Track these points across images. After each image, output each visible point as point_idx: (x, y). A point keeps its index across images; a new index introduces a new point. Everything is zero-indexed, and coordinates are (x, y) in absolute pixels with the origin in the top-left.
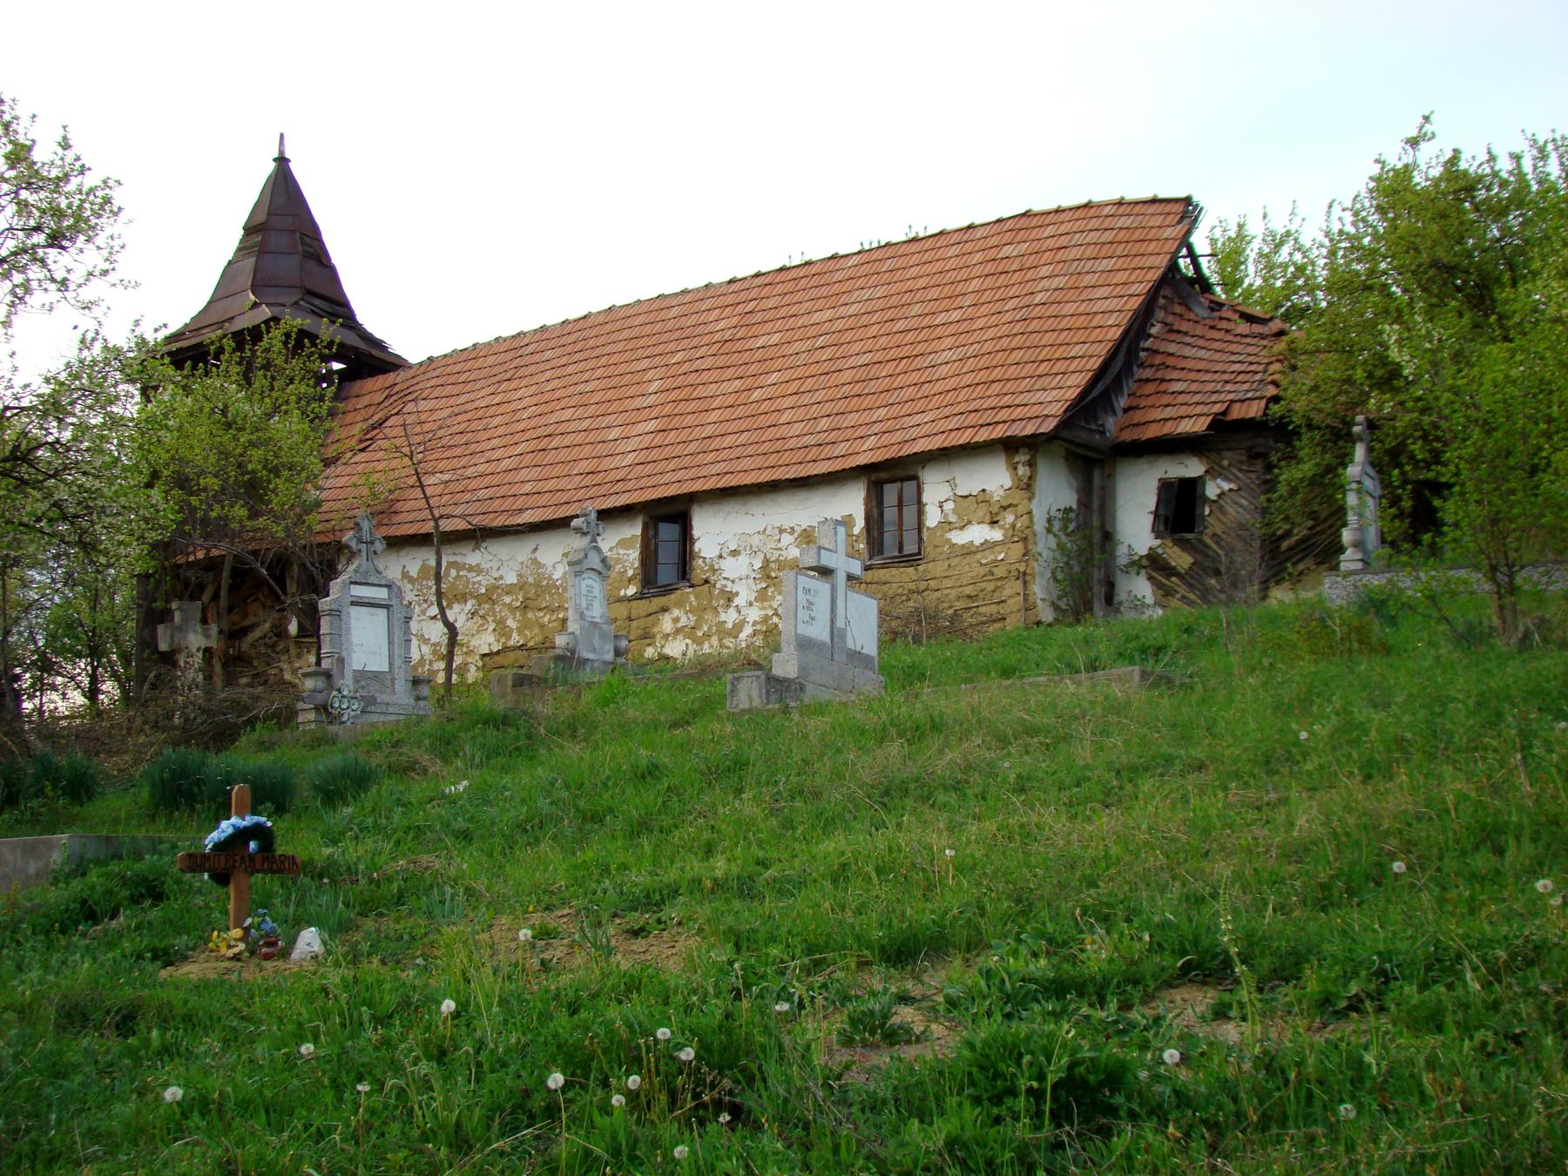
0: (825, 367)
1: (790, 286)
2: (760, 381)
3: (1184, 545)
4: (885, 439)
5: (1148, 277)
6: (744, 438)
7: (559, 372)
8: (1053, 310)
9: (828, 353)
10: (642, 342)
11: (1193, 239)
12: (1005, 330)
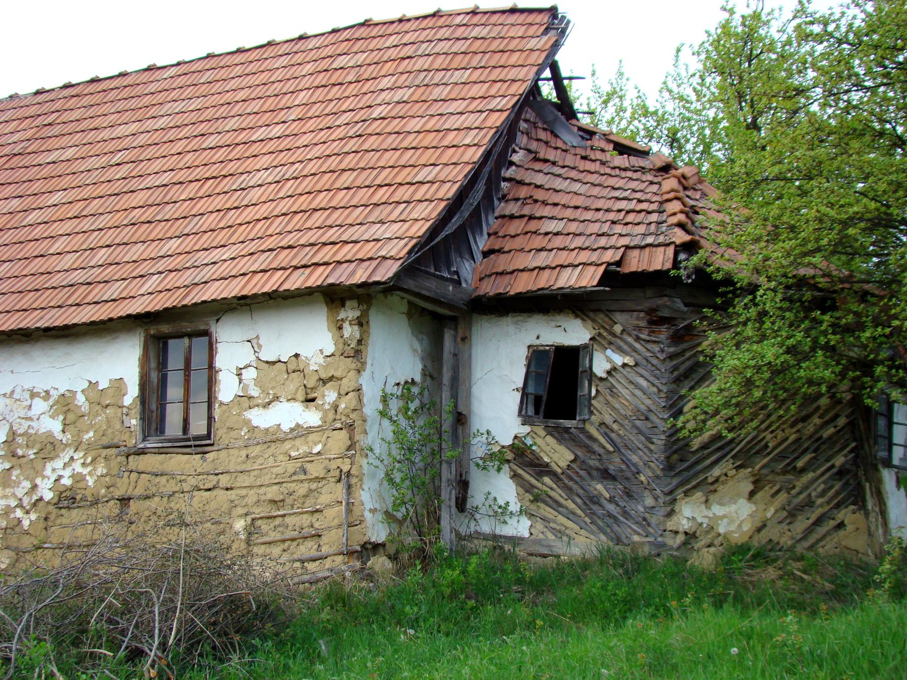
0: (117, 187)
1: (97, 98)
2: (42, 201)
3: (562, 435)
4: (172, 280)
5: (512, 90)
8: (395, 125)
9: (123, 171)
11: (561, 57)
12: (335, 147)
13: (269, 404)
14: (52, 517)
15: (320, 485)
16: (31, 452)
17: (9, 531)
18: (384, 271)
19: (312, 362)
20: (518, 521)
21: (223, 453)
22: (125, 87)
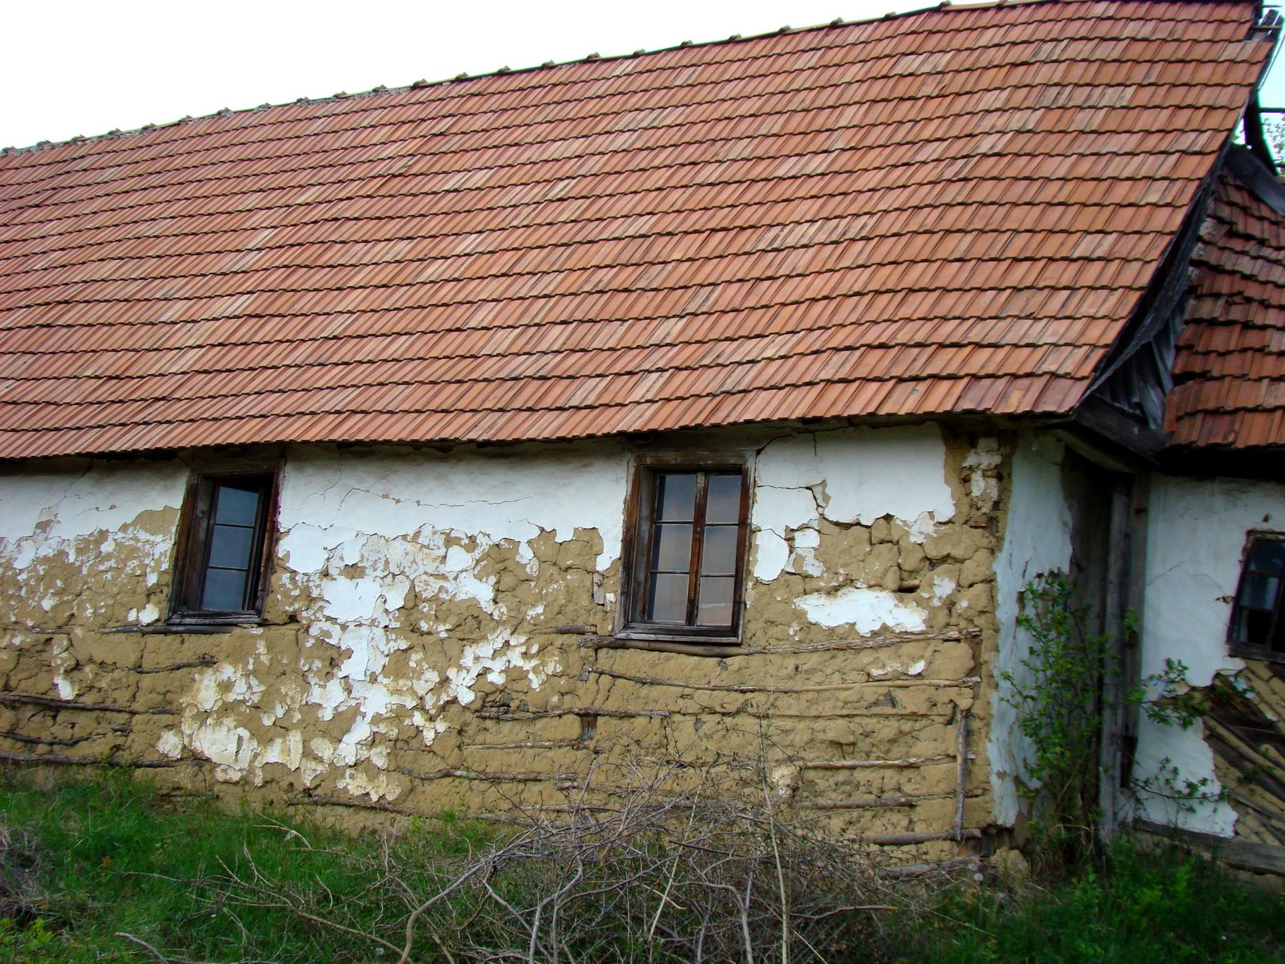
0: (564, 234)
1: (512, 100)
2: (444, 246)
4: (681, 384)
7: (115, 202)
10: (258, 167)
13: (836, 589)
14: (471, 730)
15: (918, 725)
16: (442, 628)
17: (400, 744)
18: (1060, 397)
19: (914, 530)
20: (1215, 811)
21: (756, 661)
22: (555, 85)
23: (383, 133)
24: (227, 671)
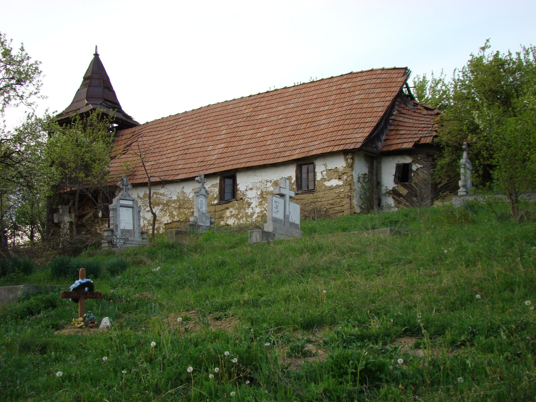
0: (282, 126)
1: (270, 98)
2: (260, 130)
3: (405, 186)
4: (303, 150)
5: (392, 95)
6: (254, 150)
8: (360, 106)
9: (283, 121)
10: (220, 117)
12: (343, 113)
23: (244, 108)
24: (231, 209)
